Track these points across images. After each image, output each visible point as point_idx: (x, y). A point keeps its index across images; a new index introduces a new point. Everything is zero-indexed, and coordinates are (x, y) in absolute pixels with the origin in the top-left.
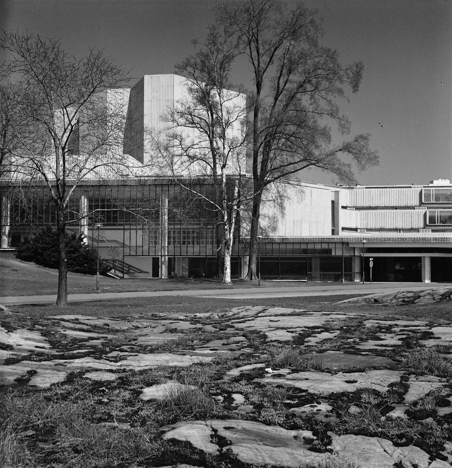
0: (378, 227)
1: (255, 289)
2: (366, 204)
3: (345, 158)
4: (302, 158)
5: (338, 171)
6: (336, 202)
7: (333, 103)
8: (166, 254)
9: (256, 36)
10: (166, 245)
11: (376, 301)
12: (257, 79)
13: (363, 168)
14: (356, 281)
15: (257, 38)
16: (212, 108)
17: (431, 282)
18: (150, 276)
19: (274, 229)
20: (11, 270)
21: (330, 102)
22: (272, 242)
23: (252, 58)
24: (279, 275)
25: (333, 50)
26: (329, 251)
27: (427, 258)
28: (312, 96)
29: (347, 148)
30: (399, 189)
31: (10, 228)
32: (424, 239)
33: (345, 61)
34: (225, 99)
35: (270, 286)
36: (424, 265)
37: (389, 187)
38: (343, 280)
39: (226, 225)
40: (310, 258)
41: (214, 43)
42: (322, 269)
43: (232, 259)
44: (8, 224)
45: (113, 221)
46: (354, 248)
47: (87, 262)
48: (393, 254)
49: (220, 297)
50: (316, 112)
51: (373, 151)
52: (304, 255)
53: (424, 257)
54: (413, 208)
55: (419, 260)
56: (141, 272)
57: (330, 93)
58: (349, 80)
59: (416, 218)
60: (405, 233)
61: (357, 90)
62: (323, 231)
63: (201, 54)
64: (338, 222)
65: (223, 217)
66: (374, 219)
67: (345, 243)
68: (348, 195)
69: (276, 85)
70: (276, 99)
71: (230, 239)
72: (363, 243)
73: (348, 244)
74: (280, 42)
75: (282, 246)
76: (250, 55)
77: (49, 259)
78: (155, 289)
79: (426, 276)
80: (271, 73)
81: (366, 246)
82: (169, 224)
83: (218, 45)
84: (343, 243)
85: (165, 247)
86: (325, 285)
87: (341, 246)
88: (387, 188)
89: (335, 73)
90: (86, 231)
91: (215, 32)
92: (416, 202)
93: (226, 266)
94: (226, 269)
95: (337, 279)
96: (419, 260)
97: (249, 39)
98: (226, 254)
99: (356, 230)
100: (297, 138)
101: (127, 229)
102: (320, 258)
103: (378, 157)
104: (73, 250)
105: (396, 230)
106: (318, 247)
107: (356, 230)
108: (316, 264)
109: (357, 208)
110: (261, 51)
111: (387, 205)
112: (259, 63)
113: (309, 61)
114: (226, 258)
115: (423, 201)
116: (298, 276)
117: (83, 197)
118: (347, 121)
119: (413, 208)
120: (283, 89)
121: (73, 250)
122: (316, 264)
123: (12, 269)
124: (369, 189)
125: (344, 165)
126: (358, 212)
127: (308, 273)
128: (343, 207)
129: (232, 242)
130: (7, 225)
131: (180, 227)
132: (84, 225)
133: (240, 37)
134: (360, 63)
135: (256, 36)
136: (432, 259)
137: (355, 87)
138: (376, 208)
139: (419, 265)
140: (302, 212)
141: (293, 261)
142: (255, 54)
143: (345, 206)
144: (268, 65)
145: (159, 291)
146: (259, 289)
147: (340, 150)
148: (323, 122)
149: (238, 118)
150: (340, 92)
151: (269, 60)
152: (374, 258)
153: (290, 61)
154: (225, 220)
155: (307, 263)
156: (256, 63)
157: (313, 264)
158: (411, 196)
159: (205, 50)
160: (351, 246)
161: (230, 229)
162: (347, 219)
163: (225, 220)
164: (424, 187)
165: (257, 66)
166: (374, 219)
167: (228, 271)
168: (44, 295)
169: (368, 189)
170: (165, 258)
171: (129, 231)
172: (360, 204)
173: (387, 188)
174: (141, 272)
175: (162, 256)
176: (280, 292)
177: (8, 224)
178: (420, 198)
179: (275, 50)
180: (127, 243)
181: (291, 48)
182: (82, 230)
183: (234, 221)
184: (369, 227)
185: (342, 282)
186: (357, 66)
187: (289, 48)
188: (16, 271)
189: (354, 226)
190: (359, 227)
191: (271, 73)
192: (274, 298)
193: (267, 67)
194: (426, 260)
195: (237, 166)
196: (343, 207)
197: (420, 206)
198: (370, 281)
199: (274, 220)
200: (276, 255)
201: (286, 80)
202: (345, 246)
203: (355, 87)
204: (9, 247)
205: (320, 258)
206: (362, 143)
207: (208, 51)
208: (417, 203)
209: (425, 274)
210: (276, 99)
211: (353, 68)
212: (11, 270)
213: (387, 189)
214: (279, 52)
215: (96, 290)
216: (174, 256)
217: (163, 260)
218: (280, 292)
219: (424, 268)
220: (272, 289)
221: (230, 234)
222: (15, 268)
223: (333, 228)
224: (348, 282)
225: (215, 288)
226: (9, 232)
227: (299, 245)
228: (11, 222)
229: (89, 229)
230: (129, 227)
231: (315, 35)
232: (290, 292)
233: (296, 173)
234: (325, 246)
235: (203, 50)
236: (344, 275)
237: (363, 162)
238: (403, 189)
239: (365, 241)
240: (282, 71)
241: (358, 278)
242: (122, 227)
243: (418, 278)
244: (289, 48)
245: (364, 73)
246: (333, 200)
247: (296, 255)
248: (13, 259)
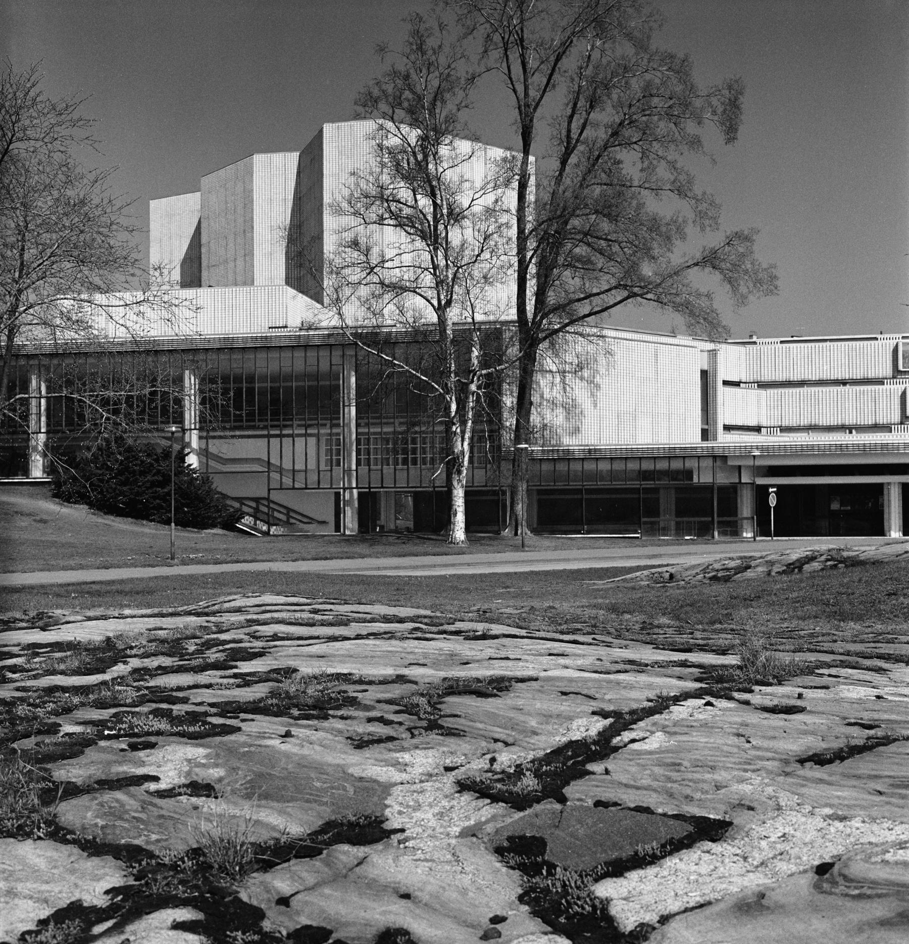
0: (805, 422)
1: (512, 554)
2: (781, 377)
3: (704, 280)
4: (613, 282)
5: (685, 308)
6: (710, 374)
7: (678, 165)
8: (354, 486)
9: (520, 32)
10: (354, 467)
11: (672, 576)
12: (522, 122)
13: (742, 300)
14: (745, 535)
15: (522, 36)
16: (431, 185)
17: (904, 535)
18: (329, 530)
19: (576, 431)
20: (35, 520)
21: (672, 165)
22: (567, 457)
23: (510, 78)
24: (582, 524)
25: (681, 55)
26: (689, 474)
27: (894, 484)
28: (643, 153)
29: (710, 260)
30: (850, 343)
31: (48, 439)
32: (884, 446)
33: (707, 77)
34: (445, 165)
35: (547, 548)
36: (889, 501)
37: (831, 340)
38: (716, 534)
39: (454, 424)
40: (656, 490)
41: (420, 48)
42: (679, 513)
43: (467, 494)
44: (43, 430)
45: (271, 420)
46: (740, 467)
47: (197, 506)
48: (780, 478)
49: (402, 573)
50: (647, 185)
51: (765, 266)
52: (649, 484)
53: (889, 484)
54: (879, 382)
55: (879, 489)
56: (311, 521)
57: (672, 147)
58: (716, 118)
59: (884, 404)
60: (859, 435)
61: (734, 139)
62: (685, 433)
63: (395, 73)
64: (715, 413)
65: (448, 408)
66: (796, 407)
67: (720, 459)
68: (743, 357)
69: (564, 132)
70: (564, 162)
71: (463, 452)
72: (754, 456)
73: (724, 458)
74: (566, 45)
76: (507, 72)
77: (112, 498)
78: (295, 556)
79: (893, 522)
80: (554, 106)
81: (758, 463)
82: (358, 425)
83: (430, 52)
84: (715, 457)
85: (351, 470)
86: (678, 545)
87: (709, 462)
88: (826, 340)
89: (686, 105)
90: (194, 440)
91: (422, 27)
92: (886, 370)
93: (454, 507)
94: (455, 515)
95: (703, 531)
96: (879, 489)
97: (503, 38)
98: (455, 483)
99: (757, 429)
100: (611, 240)
101: (288, 436)
102: (676, 488)
103: (775, 277)
104: (161, 478)
105: (842, 428)
106: (662, 465)
107: (757, 429)
108: (667, 502)
109: (763, 385)
110: (532, 63)
111: (825, 376)
112: (526, 88)
113: (634, 82)
114: (455, 492)
115: (901, 368)
116: (616, 527)
117: (187, 372)
118: (712, 204)
119: (879, 382)
120: (578, 141)
121: (161, 478)
122: (667, 502)
123: (38, 518)
124: (788, 345)
125: (699, 295)
126: (763, 392)
127: (643, 520)
128: (726, 383)
129: (466, 458)
130: (40, 432)
131: (379, 430)
132: (191, 429)
133: (488, 36)
134: (736, 81)
135: (520, 32)
137: (731, 131)
138: (802, 384)
139: (880, 500)
140: (628, 393)
141: (623, 496)
142: (517, 69)
143: (737, 380)
144: (544, 91)
145: (303, 560)
146: (522, 554)
147: (696, 264)
148: (662, 206)
149: (474, 202)
150: (695, 143)
151: (545, 81)
152: (779, 487)
153: (592, 81)
154: (453, 414)
155: (582, 499)
156: (520, 88)
157: (661, 501)
158: (875, 357)
159: (402, 65)
160: (730, 463)
161: (463, 432)
163: (453, 414)
164: (903, 338)
165: (522, 96)
166: (796, 407)
167: (460, 518)
169: (784, 345)
170: (351, 494)
171: (266, 439)
172: (767, 377)
173: (826, 340)
174: (311, 521)
175: (344, 489)
176: (590, 559)
177: (43, 430)
178: (893, 361)
179: (558, 59)
180: (275, 460)
181: (596, 55)
182: (187, 440)
183: (470, 415)
184: (786, 423)
185: (713, 537)
186: (730, 88)
187: (590, 55)
188: (44, 522)
189: (753, 423)
190: (764, 424)
191: (554, 106)
192: (481, 575)
193: (542, 97)
194: (892, 492)
195: (496, 300)
196: (726, 383)
197: (894, 377)
198: (770, 536)
199: (571, 409)
200: (574, 485)
201: (582, 121)
202: (719, 463)
203: (731, 131)
204: (45, 476)
205: (676, 488)
206: (741, 250)
207: (408, 67)
208: (889, 372)
209: (889, 519)
210: (564, 162)
211: (723, 92)
212: (35, 520)
213: (824, 344)
214: (570, 63)
215: (170, 558)
216: (370, 488)
217: (347, 497)
218: (590, 559)
219: (889, 506)
220: (549, 555)
221: (463, 440)
222: (45, 517)
223: (706, 427)
224: (723, 538)
225: (426, 554)
226: (46, 445)
227: (653, 461)
228: (48, 425)
229: (200, 438)
230: (304, 432)
231: (646, 26)
232: (575, 559)
233: (605, 314)
234: (676, 465)
235: (396, 65)
236: (719, 522)
237: (743, 289)
238: (858, 343)
239: (757, 453)
240: (575, 104)
241: (749, 529)
242: (265, 432)
244: (590, 55)
245: (745, 101)
246: (706, 368)
247: (618, 484)
248: (46, 498)
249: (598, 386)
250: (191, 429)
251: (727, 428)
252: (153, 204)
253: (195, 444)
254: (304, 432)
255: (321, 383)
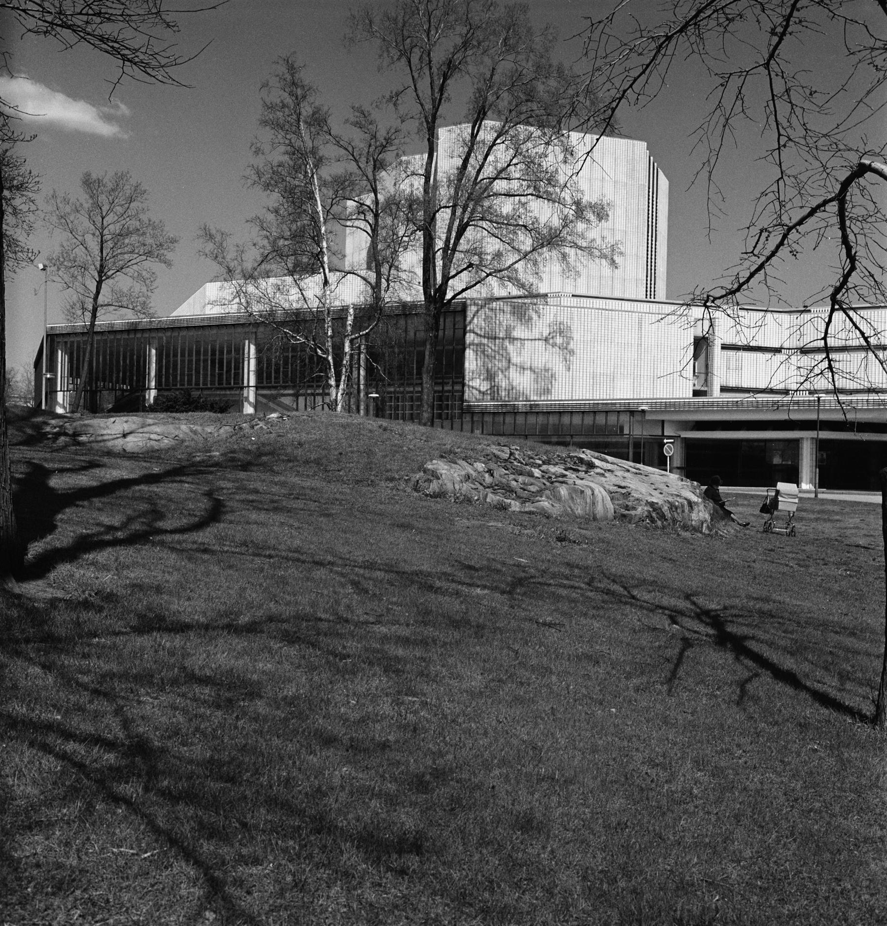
27: (807, 440)
46: (663, 422)
53: (802, 438)
55: (797, 442)
62: (681, 389)
71: (336, 400)
75: (532, 419)
84: (632, 413)
96: (797, 442)
101: (318, 394)
128: (725, 347)
136: (822, 445)
160: (649, 417)
161: (338, 386)
162: (727, 370)
168: (114, 457)
196: (725, 347)
243: (227, 406)
249: (572, 352)
250: (249, 386)
251: (724, 389)
252: (640, 147)
253: (252, 398)
254: (441, 388)
255: (446, 347)
